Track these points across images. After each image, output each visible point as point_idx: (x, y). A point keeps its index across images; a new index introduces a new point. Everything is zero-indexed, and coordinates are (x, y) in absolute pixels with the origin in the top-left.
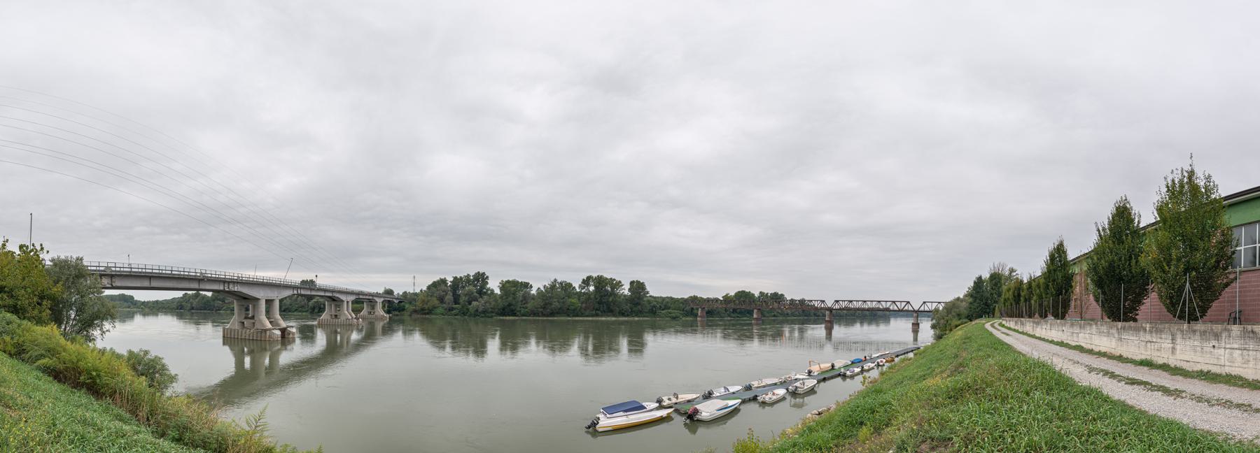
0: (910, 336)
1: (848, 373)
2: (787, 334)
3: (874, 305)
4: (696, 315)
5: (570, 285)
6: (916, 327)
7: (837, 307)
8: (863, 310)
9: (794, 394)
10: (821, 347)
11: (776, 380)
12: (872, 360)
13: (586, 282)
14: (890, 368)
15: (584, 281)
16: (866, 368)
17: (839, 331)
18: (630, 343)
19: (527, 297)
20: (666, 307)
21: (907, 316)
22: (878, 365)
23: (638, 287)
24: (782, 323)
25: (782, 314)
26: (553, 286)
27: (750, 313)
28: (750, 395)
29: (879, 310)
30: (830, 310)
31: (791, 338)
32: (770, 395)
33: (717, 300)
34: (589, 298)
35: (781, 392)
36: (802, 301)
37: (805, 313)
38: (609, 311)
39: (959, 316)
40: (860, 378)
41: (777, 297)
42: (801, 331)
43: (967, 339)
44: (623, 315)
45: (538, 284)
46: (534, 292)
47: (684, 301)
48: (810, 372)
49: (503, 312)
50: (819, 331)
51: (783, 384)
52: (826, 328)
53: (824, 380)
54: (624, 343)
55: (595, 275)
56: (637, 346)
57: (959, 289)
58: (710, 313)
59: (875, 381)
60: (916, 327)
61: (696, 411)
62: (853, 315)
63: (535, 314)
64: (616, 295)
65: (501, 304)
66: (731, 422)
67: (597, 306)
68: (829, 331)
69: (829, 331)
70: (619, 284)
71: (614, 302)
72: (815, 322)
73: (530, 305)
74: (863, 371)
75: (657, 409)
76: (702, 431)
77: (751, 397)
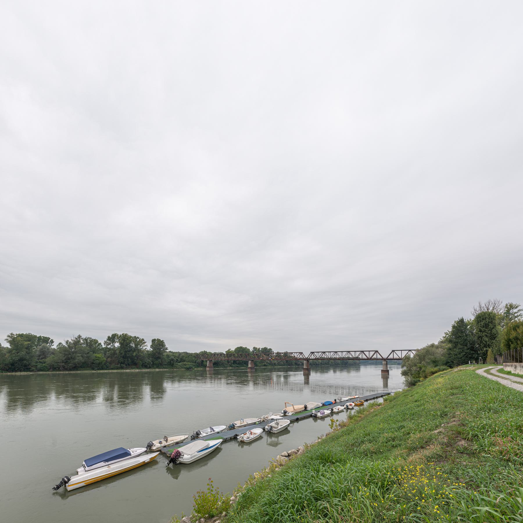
0: (380, 382)
1: (319, 415)
2: (275, 379)
3: (344, 355)
4: (205, 366)
5: (96, 341)
6: (385, 374)
7: (312, 357)
8: (335, 359)
9: (270, 433)
10: (301, 390)
11: (256, 420)
12: (342, 403)
13: (112, 339)
14: (359, 412)
15: (109, 338)
16: (335, 410)
17: (314, 376)
18: (152, 390)
19: (44, 353)
20: (182, 360)
21: (376, 364)
22: (347, 408)
23: (158, 344)
24: (271, 371)
25: (271, 364)
26: (77, 342)
27: (246, 363)
28: (231, 434)
29: (349, 359)
30: (307, 360)
31: (278, 383)
32: (248, 435)
33: (221, 354)
34: (115, 353)
35: (258, 431)
36: (286, 354)
37: (288, 363)
38: (134, 364)
39: (435, 363)
40: (328, 420)
41: (267, 351)
42: (286, 377)
43: (456, 389)
44: (146, 367)
45: (59, 339)
46: (55, 346)
47: (197, 355)
48: (285, 412)
49: (12, 367)
50: (297, 377)
51: (262, 423)
52: (304, 375)
53: (297, 420)
54: (147, 390)
55: (120, 333)
56: (158, 390)
57: (434, 334)
58: (216, 364)
59: (342, 425)
60: (385, 374)
61: (179, 455)
62: (328, 364)
63: (54, 369)
64: (140, 351)
65: (8, 358)
66: (213, 463)
67: (121, 360)
68: (307, 376)
69: (307, 376)
70: (142, 342)
71: (137, 356)
72: (297, 370)
73: (49, 360)
74: (332, 413)
75: (146, 452)
76: (184, 474)
77: (232, 437)
